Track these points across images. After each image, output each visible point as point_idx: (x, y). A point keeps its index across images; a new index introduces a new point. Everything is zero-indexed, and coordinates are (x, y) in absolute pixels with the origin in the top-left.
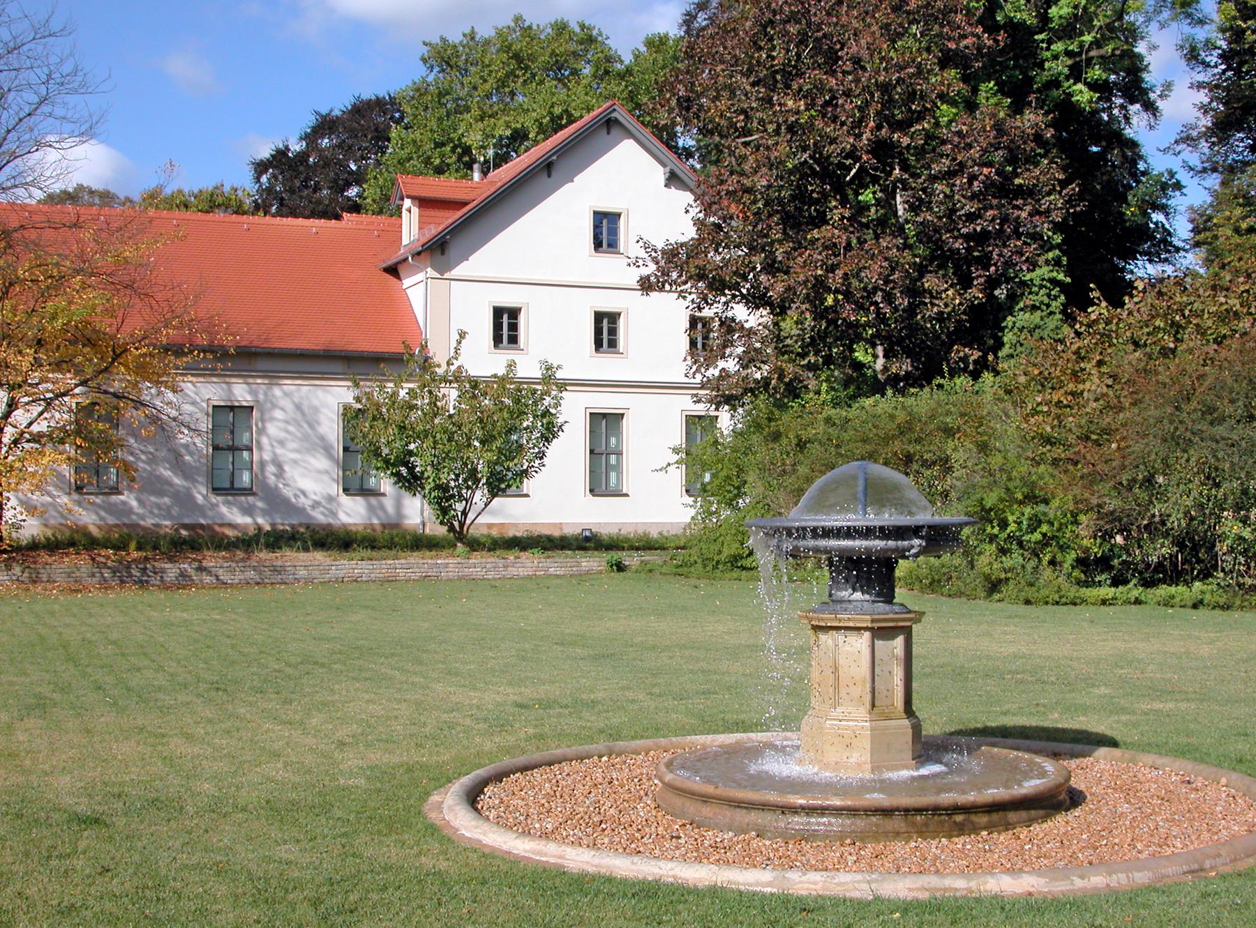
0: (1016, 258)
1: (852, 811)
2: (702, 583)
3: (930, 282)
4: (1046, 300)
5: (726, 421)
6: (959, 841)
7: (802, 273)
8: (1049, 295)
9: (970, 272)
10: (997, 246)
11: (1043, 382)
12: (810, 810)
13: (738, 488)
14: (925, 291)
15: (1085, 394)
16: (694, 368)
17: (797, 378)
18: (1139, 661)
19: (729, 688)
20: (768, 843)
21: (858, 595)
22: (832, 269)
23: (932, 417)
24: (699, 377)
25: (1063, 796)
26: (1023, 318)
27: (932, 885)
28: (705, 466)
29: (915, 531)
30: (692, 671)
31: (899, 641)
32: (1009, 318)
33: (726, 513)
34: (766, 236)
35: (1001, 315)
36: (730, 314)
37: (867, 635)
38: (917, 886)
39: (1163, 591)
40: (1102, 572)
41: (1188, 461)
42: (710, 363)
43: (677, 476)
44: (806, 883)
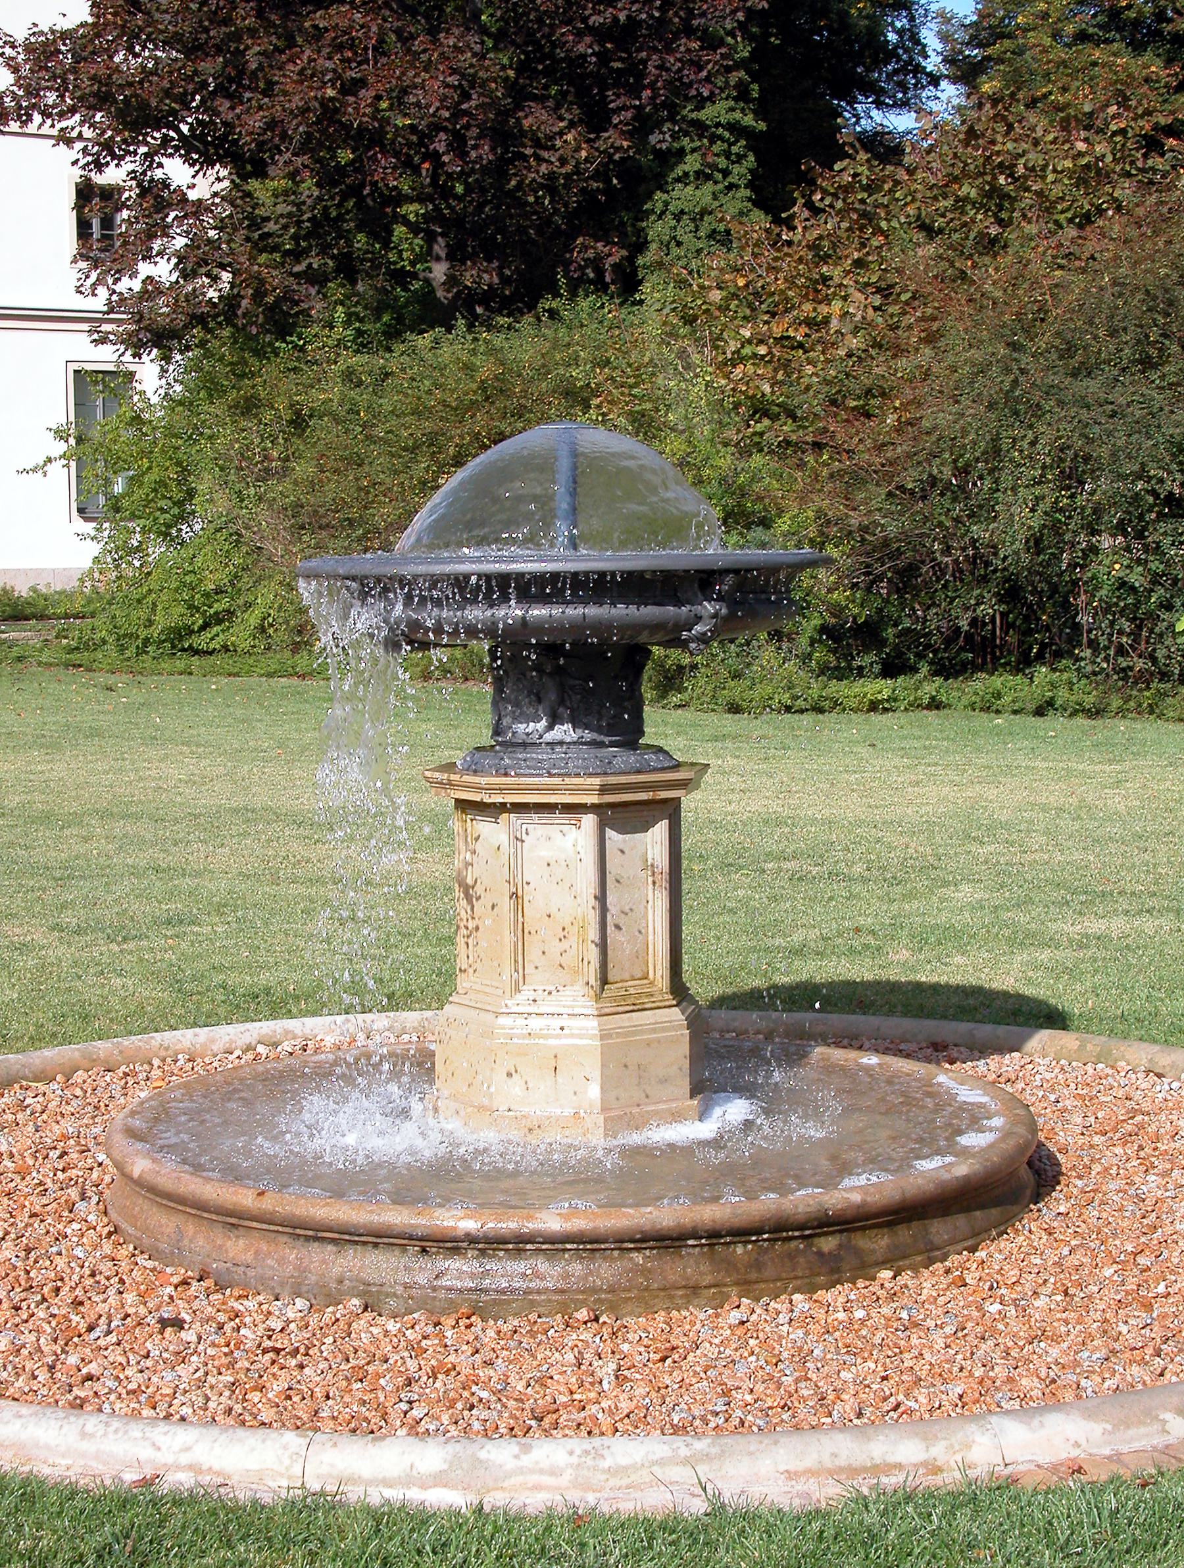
0: (689, 74)
1: (588, 1244)
2: (120, 680)
3: (536, 118)
4: (722, 163)
5: (149, 375)
6: (836, 1296)
7: (295, 95)
8: (727, 154)
9: (604, 100)
10: (655, 49)
11: (754, 301)
12: (487, 1245)
13: (180, 504)
14: (522, 133)
15: (834, 324)
16: (94, 276)
17: (288, 296)
18: (1006, 826)
19: (219, 909)
20: (392, 1326)
21: (564, 731)
22: (351, 88)
23: (543, 371)
24: (103, 292)
25: (1025, 1173)
26: (684, 196)
27: (842, 1462)
28: (116, 464)
29: (704, 580)
30: (134, 871)
31: (660, 830)
32: (658, 195)
33: (156, 550)
34: (227, 22)
35: (642, 189)
36: (159, 174)
37: (589, 821)
38: (809, 1462)
39: (981, 684)
40: (866, 649)
41: (1033, 443)
42: (126, 268)
43: (60, 483)
44: (537, 1475)
